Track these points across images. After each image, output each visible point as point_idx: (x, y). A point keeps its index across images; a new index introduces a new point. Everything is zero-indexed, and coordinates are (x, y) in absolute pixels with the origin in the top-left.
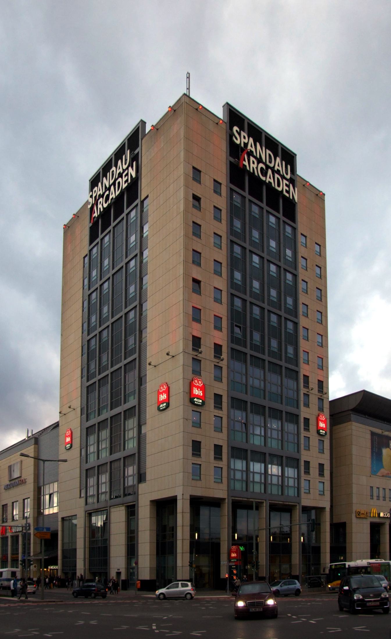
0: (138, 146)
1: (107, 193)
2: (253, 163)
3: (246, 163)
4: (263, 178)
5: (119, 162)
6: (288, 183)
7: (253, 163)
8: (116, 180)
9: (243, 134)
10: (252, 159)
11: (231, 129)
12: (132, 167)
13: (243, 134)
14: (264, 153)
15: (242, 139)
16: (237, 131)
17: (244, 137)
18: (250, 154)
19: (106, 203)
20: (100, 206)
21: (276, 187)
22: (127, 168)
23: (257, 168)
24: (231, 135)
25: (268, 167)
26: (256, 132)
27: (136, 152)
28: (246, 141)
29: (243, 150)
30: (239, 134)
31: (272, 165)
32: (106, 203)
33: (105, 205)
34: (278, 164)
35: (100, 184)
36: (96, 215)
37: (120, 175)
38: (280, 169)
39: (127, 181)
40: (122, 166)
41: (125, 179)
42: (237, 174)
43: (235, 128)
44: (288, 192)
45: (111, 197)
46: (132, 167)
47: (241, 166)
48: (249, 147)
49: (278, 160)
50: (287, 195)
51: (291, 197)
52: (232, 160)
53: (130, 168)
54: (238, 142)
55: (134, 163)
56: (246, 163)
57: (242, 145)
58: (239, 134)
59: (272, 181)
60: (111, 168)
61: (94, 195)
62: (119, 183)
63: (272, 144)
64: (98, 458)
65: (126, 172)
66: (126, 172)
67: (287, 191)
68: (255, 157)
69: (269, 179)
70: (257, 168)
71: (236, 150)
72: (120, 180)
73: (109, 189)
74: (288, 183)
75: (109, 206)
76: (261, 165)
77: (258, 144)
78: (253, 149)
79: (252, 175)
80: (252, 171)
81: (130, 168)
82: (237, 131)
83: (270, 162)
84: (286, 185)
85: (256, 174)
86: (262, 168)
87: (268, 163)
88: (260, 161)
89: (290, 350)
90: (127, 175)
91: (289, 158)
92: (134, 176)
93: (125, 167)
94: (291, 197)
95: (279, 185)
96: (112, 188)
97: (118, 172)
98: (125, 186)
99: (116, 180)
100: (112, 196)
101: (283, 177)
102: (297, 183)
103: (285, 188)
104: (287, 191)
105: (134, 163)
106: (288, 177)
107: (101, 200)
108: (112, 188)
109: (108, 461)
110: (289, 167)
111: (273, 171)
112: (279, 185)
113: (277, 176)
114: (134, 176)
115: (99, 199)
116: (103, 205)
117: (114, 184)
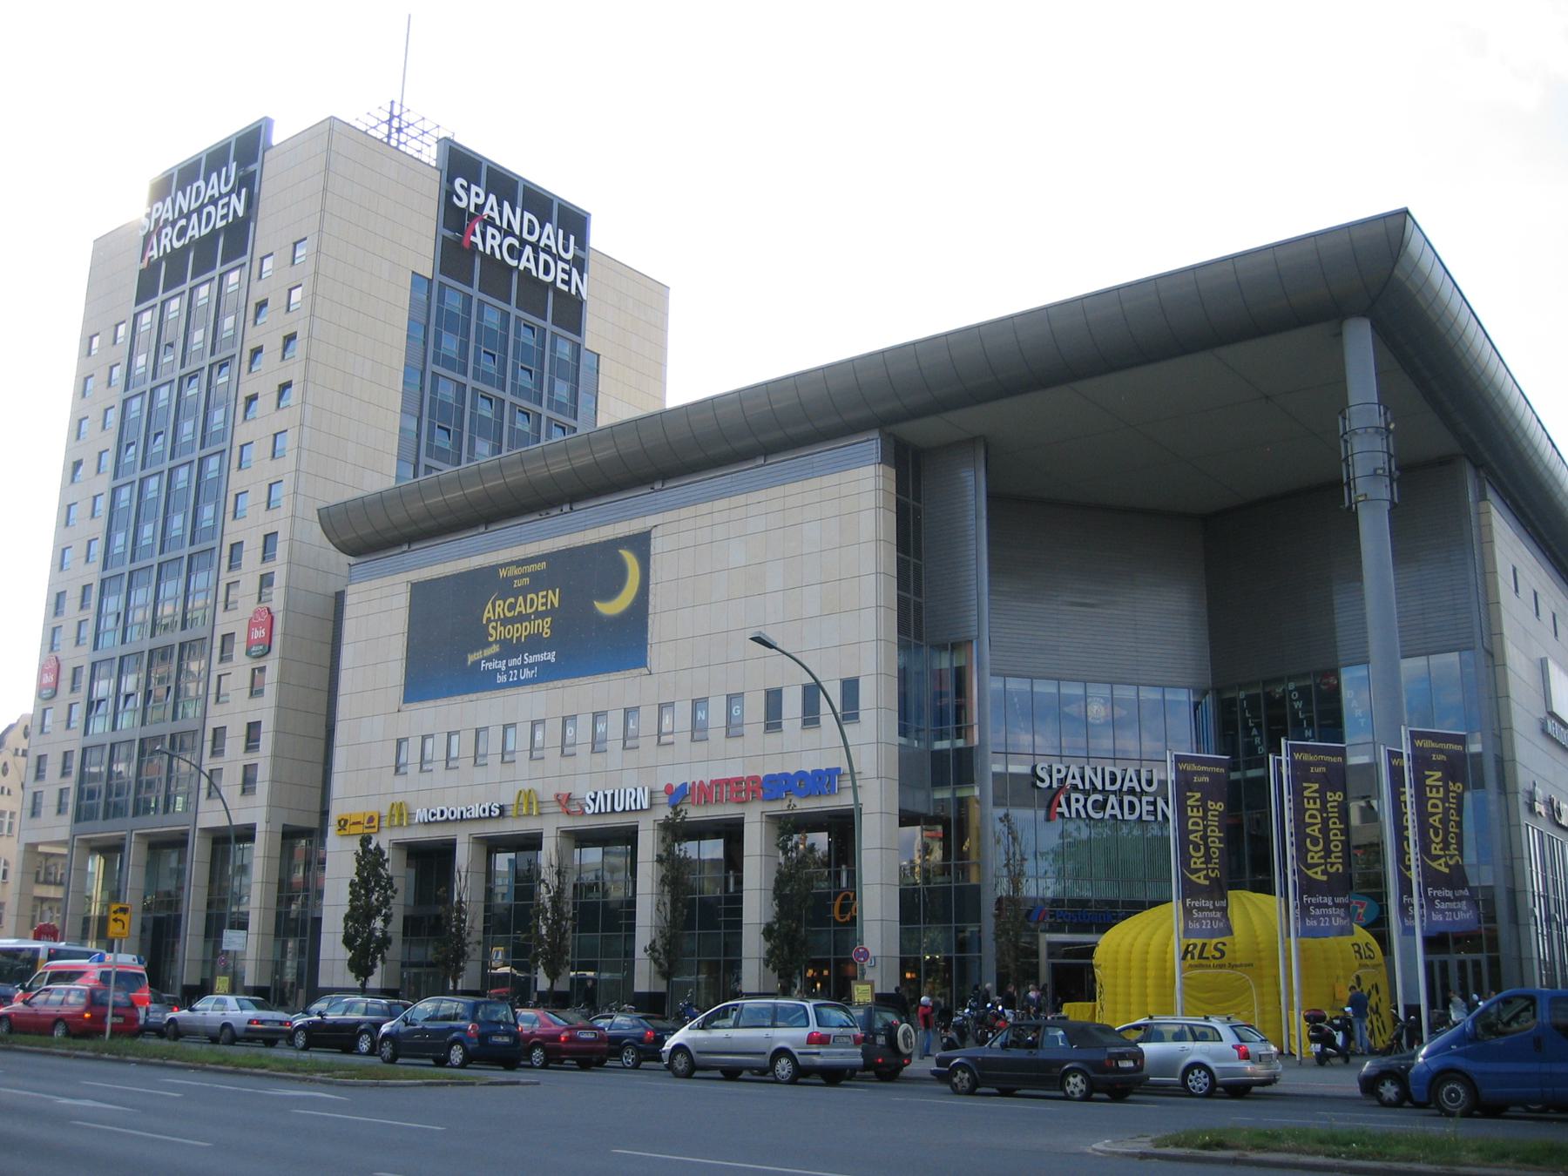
0: (256, 160)
1: (183, 222)
2: (493, 237)
3: (478, 240)
4: (514, 263)
5: (214, 176)
6: (567, 267)
7: (493, 237)
8: (203, 206)
9: (474, 188)
10: (490, 230)
11: (451, 181)
12: (239, 196)
13: (474, 188)
14: (519, 219)
15: (471, 197)
16: (460, 199)
17: (477, 195)
18: (490, 222)
19: (179, 239)
20: (165, 241)
21: (541, 276)
22: (229, 194)
23: (500, 246)
24: (450, 193)
25: (523, 242)
26: (503, 184)
27: (251, 168)
28: (481, 201)
29: (472, 217)
30: (468, 190)
31: (533, 239)
32: (179, 239)
33: (177, 245)
34: (549, 235)
35: (169, 200)
36: (154, 253)
37: (213, 201)
38: (552, 243)
39: (224, 217)
40: (216, 185)
41: (221, 212)
42: (456, 253)
43: (459, 181)
44: (567, 283)
45: (190, 233)
46: (239, 196)
47: (467, 246)
48: (487, 211)
49: (549, 228)
50: (565, 288)
51: (573, 291)
52: (449, 234)
53: (234, 196)
54: (462, 205)
55: (244, 191)
56: (478, 240)
57: (472, 209)
58: (468, 190)
59: (532, 266)
60: (197, 179)
61: (155, 216)
62: (209, 214)
63: (539, 203)
64: (86, 733)
65: (226, 200)
66: (226, 200)
67: (563, 281)
68: (499, 229)
69: (526, 261)
70: (500, 246)
71: (455, 219)
72: (211, 208)
73: (188, 217)
74: (567, 267)
75: (185, 248)
76: (510, 240)
77: (506, 204)
78: (496, 215)
79: (489, 259)
80: (488, 251)
81: (234, 196)
82: (460, 199)
83: (531, 232)
84: (564, 270)
85: (498, 256)
86: (511, 247)
87: (525, 235)
88: (509, 232)
89: (562, 390)
90: (228, 204)
91: (574, 223)
92: (240, 214)
93: (224, 190)
94: (573, 291)
95: (547, 272)
96: (195, 217)
97: (209, 193)
98: (220, 224)
99: (203, 206)
100: (193, 233)
101: (557, 258)
102: (591, 266)
103: (561, 275)
104: (563, 281)
105: (244, 191)
106: (569, 256)
107: (168, 229)
108: (195, 217)
109: (108, 741)
110: (572, 238)
111: (535, 247)
112: (547, 272)
113: (543, 256)
114: (240, 214)
115: (164, 226)
116: (169, 241)
117: (199, 210)
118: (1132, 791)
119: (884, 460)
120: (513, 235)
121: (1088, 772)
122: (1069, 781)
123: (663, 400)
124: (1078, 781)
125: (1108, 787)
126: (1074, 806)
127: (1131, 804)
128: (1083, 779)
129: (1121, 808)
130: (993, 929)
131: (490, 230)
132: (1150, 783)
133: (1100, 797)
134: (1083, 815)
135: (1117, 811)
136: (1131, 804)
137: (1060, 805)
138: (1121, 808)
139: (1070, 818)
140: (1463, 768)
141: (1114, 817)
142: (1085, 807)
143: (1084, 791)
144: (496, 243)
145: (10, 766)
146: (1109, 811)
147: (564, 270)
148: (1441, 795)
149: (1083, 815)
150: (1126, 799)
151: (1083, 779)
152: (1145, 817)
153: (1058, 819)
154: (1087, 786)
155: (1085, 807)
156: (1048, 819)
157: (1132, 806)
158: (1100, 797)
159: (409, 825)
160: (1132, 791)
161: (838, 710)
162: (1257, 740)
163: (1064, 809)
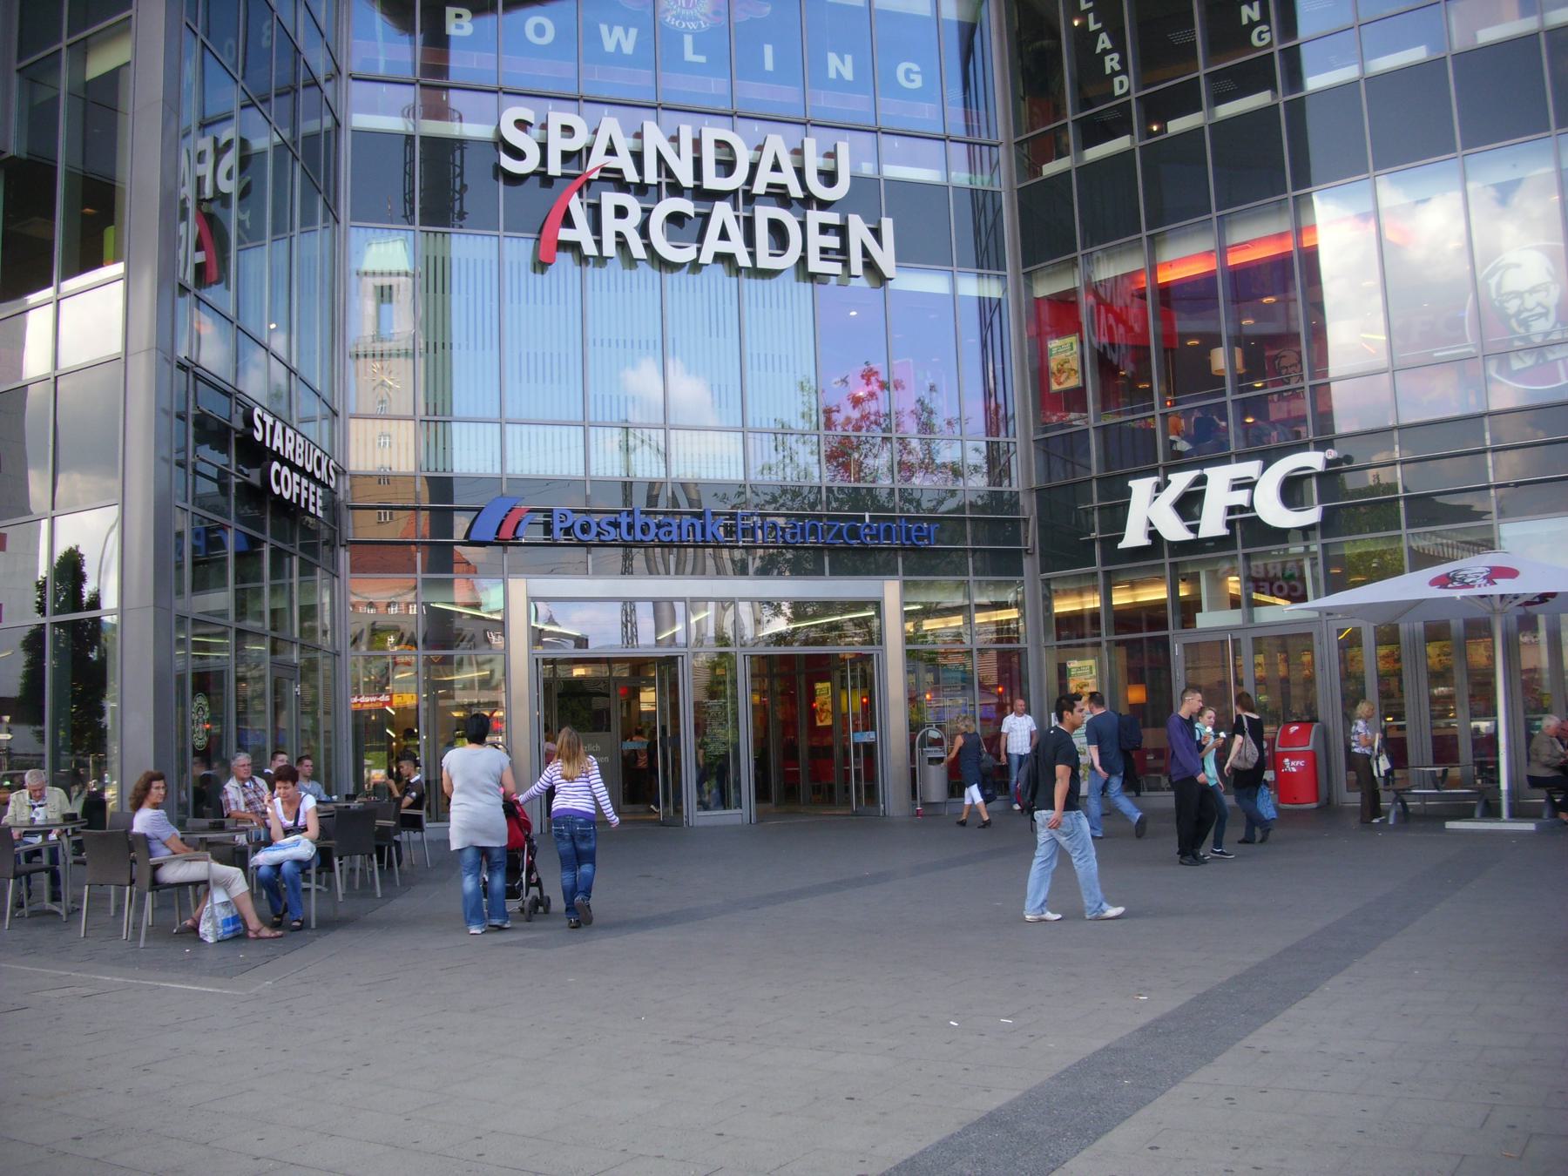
6: (833, 218)
7: (621, 212)
86: (676, 219)
113: (764, 214)
118: (779, 195)
119: (448, 37)
120: (676, 189)
121: (654, 139)
122: (598, 159)
123: (859, 8)
124: (788, 178)
125: (712, 181)
126: (610, 224)
127: (777, 228)
128: (638, 157)
129: (750, 240)
130: (212, 608)
131: (610, 200)
132: (829, 178)
133: (686, 206)
134: (638, 250)
135: (736, 245)
136: (777, 228)
137: (568, 222)
138: (750, 240)
139: (601, 260)
140: (1059, 1162)
141: (725, 259)
142: (644, 230)
143: (641, 189)
144: (629, 226)
145: (349, 641)
146: (712, 244)
147: (824, 229)
148: (815, 265)
149: (638, 250)
150: (764, 214)
151: (638, 157)
152: (815, 265)
153: (565, 260)
154: (651, 177)
155: (644, 230)
156: (541, 265)
157: (778, 231)
158: (686, 206)
159: (1047, 582)
160: (779, 195)
161: (1439, 499)
162: (1111, 63)
163: (581, 232)
